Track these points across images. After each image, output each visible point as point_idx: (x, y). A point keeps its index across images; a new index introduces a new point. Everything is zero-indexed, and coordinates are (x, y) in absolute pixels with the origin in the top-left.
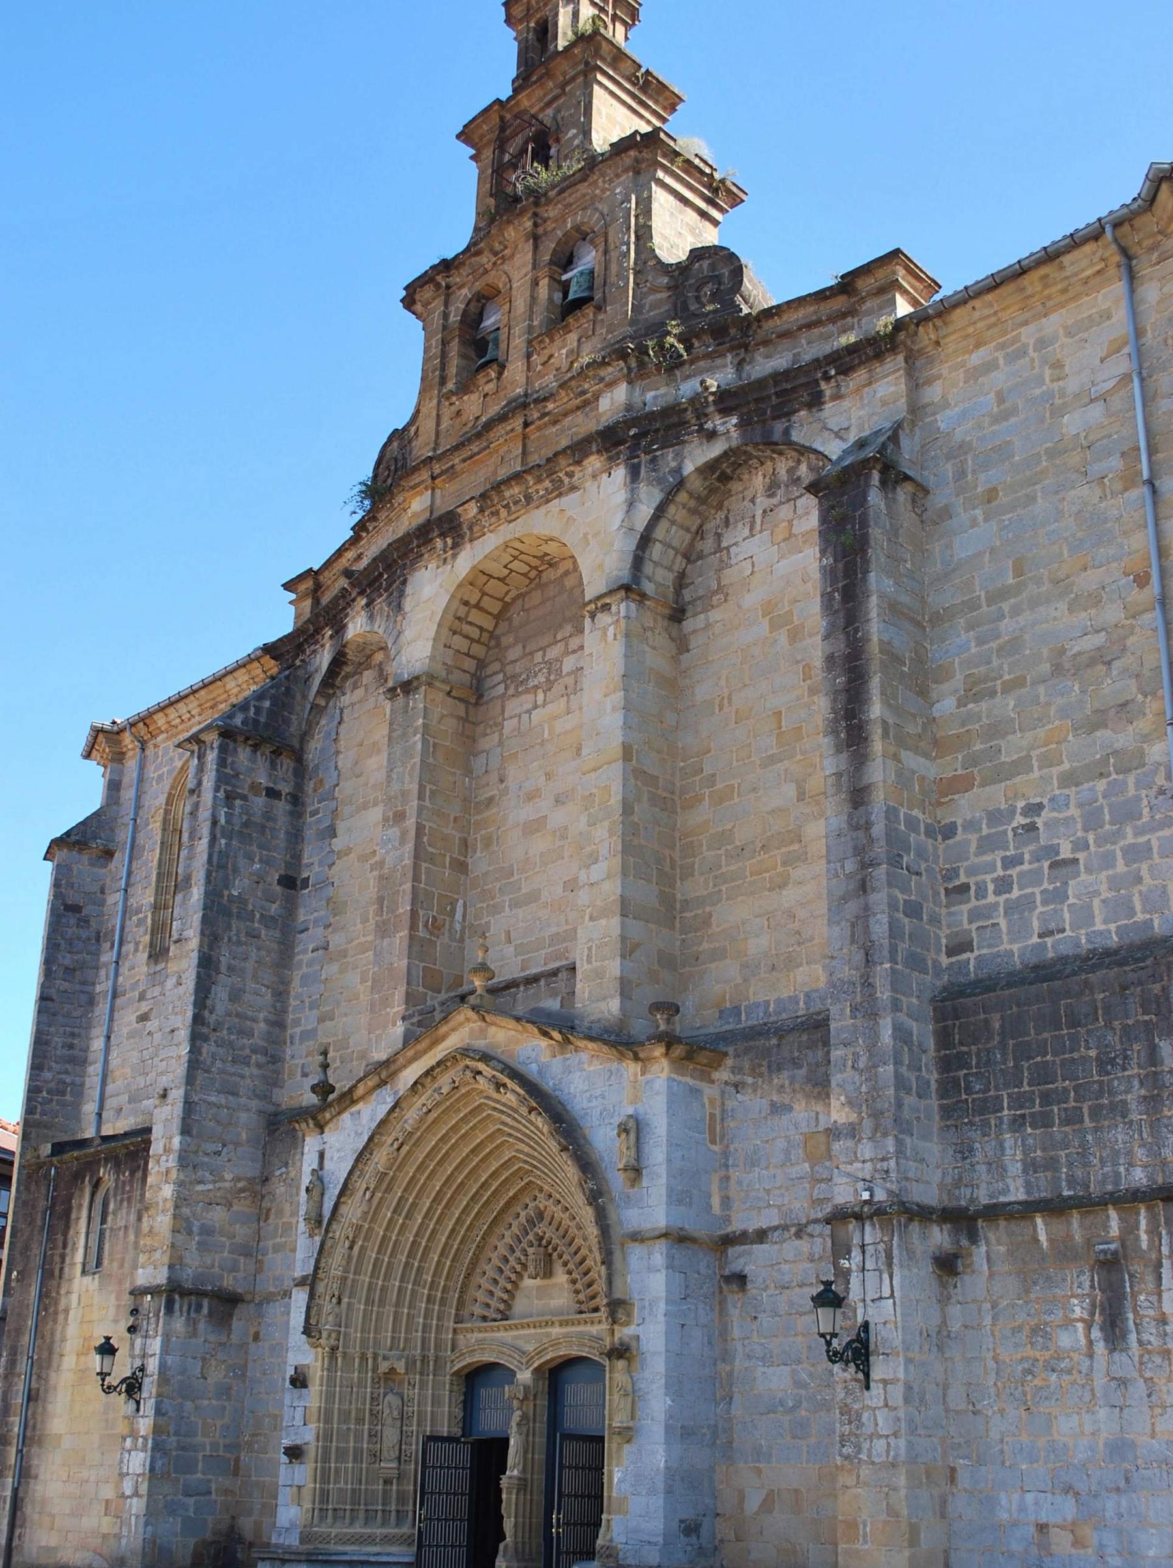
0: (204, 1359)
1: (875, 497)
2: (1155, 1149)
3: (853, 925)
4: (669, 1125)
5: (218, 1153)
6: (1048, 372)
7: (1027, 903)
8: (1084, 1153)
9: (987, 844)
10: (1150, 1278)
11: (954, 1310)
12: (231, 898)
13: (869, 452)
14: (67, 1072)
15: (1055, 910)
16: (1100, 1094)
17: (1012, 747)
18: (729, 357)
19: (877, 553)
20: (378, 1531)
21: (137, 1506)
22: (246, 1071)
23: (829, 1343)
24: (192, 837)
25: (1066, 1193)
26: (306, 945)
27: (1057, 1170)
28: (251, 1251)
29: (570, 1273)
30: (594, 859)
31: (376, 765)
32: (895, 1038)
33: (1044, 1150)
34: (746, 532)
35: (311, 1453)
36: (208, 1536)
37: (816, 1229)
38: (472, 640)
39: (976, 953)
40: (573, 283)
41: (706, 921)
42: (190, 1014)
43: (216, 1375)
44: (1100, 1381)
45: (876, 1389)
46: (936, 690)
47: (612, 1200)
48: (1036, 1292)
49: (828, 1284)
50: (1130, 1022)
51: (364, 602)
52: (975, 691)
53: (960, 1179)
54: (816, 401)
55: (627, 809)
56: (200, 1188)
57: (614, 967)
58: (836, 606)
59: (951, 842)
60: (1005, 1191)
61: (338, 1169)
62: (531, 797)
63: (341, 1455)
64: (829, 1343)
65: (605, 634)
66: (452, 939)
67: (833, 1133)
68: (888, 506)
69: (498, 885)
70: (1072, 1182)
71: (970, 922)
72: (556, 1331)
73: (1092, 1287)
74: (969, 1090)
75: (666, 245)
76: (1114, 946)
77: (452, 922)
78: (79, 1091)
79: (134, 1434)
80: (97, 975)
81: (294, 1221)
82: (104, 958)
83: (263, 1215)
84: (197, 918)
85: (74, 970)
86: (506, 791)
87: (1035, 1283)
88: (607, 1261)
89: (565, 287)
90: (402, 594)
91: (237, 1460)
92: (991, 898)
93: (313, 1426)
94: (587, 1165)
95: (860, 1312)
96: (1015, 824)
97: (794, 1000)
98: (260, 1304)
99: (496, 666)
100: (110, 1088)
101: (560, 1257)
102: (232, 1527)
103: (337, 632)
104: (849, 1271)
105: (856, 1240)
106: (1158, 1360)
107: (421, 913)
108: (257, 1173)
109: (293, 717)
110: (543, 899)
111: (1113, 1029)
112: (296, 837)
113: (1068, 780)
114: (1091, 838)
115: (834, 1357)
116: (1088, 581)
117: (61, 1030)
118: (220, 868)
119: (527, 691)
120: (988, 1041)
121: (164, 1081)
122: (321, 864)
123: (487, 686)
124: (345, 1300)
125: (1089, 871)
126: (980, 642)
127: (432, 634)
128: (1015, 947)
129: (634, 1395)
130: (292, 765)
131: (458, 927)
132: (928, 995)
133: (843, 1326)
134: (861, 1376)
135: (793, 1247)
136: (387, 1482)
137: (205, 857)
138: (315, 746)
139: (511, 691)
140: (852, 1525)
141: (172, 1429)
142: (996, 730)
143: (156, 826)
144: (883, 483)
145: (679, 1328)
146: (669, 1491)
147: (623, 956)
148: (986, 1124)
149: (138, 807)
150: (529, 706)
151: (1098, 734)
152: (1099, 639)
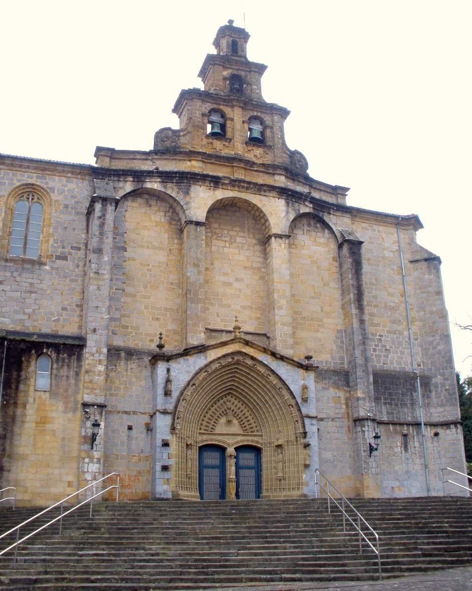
2: (413, 413)
17: (376, 320)
44: (403, 458)
60: (383, 418)
69: (212, 297)
72: (240, 438)
104: (365, 431)
105: (366, 424)
113: (389, 332)
140: (368, 487)
150: (223, 246)
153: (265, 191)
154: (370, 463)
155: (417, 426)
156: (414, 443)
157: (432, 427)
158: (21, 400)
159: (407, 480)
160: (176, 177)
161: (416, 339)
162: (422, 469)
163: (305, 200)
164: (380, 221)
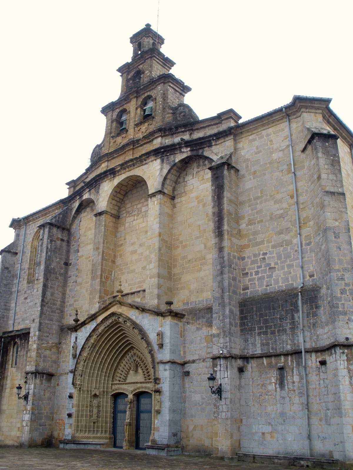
0: (44, 390)
1: (226, 172)
2: (293, 340)
3: (219, 283)
4: (170, 333)
5: (48, 336)
6: (269, 143)
7: (263, 278)
8: (275, 341)
9: (253, 262)
10: (291, 372)
11: (243, 381)
12: (51, 269)
13: (224, 160)
14: (5, 312)
15: (270, 280)
16: (280, 327)
18: (188, 132)
19: (226, 187)
20: (92, 436)
21: (27, 429)
22: (55, 315)
23: (212, 389)
24: (41, 251)
25: (271, 351)
26: (71, 281)
27: (269, 346)
28: (56, 362)
29: (142, 370)
30: (150, 262)
31: (91, 234)
32: (229, 312)
33: (266, 340)
34: (192, 177)
35: (74, 415)
36: (45, 437)
37: (208, 360)
38: (117, 202)
39: (250, 290)
40: (147, 110)
41: (180, 279)
42: (40, 299)
43: (47, 395)
44: (278, 397)
45: (223, 400)
46: (241, 222)
47: (155, 352)
48: (263, 376)
49: (212, 374)
50: (288, 309)
51: (88, 190)
52: (251, 222)
53: (245, 347)
54: (210, 146)
55: (160, 249)
56: (43, 345)
57: (156, 291)
58: (216, 200)
59: (244, 261)
61: (81, 342)
62: (133, 244)
63: (82, 416)
64: (212, 389)
65: (154, 203)
66: (111, 281)
67: (213, 336)
68: (229, 174)
70: (272, 348)
71: (249, 282)
73: (277, 374)
74: (247, 325)
75: (171, 102)
76: (284, 290)
77: (111, 277)
78: (8, 317)
79: (26, 410)
80: (13, 286)
81: (68, 354)
82: (15, 282)
83: (59, 353)
84: (42, 273)
85: (7, 285)
86: (126, 242)
87: (263, 374)
88: (154, 368)
89: (145, 111)
90: (99, 189)
91: (53, 417)
92: (254, 276)
93: (75, 408)
94: (148, 343)
95: (219, 381)
96: (260, 258)
97: (203, 301)
98: (59, 376)
99: (124, 209)
100: (16, 317)
101: (140, 365)
102: (52, 434)
103: (80, 197)
104: (217, 371)
105: (219, 363)
106: (292, 392)
107: (103, 274)
108: (58, 342)
109: (68, 219)
110: (136, 272)
111: (283, 310)
112: (68, 252)
113: (273, 247)
114: (279, 262)
115: (213, 392)
116: (279, 197)
117: (3, 301)
118: (49, 260)
119: (132, 216)
120: (252, 313)
121: (34, 317)
122: (75, 259)
123: (121, 214)
124: (83, 376)
125: (278, 270)
126: (252, 210)
127: (107, 200)
128: (260, 289)
129: (160, 402)
130: (67, 232)
131: (113, 278)
132: (237, 301)
133: (216, 385)
134: (219, 397)
135: (202, 364)
136: (94, 423)
137: (45, 257)
138: (74, 227)
139: (128, 215)
141: (36, 408)
142: (255, 233)
143: (29, 247)
144: (228, 169)
145: (172, 385)
146: (170, 426)
147: (158, 288)
148: (251, 334)
149: (24, 241)
150: (132, 220)
151: (281, 235)
152: (282, 211)
153: (146, 160)
154: (220, 407)
155: (297, 355)
156: (294, 378)
157: (319, 354)
158: (5, 376)
159: (282, 424)
160: (93, 183)
161: (308, 244)
162: (302, 410)
163: (181, 148)
164: (268, 124)
